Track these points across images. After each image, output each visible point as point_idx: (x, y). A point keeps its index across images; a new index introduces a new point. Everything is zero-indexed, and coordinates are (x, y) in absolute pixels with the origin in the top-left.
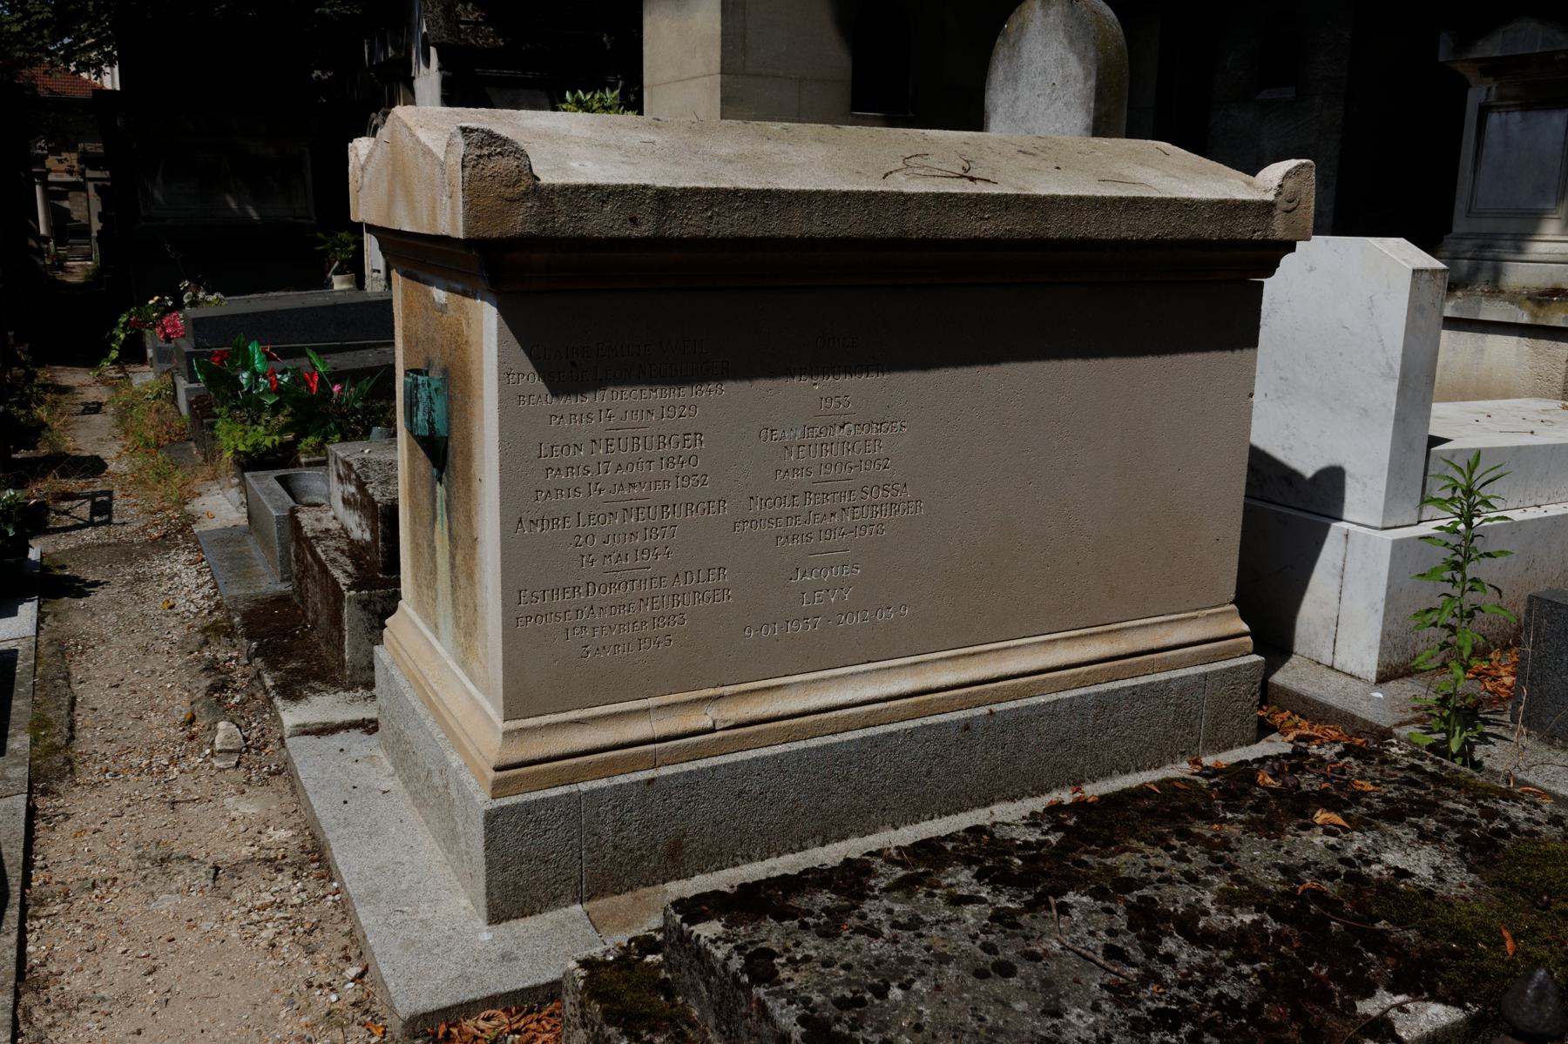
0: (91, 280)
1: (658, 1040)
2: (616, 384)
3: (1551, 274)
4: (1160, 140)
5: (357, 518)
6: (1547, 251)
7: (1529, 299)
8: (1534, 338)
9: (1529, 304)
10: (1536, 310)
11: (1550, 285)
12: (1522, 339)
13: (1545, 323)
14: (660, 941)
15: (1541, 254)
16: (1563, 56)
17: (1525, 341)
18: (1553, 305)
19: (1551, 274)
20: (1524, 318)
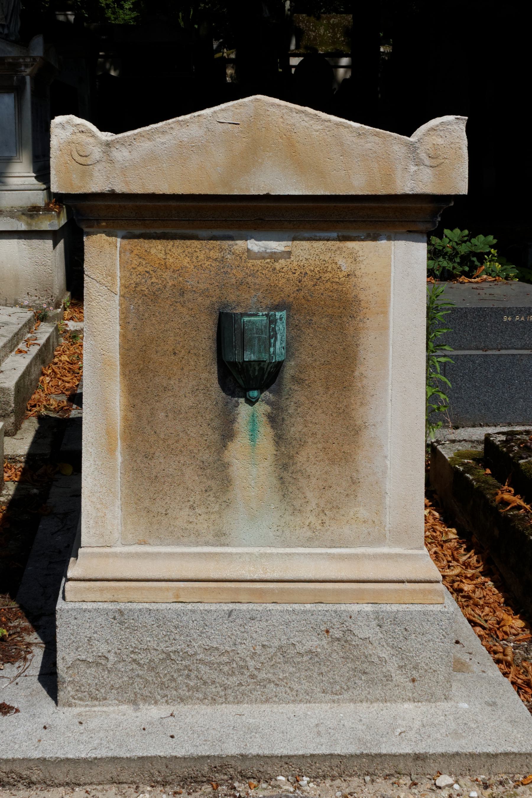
0: (524, 497)
1: (402, 795)
2: (83, 256)
3: (29, 198)
4: (264, 95)
5: (169, 787)
6: (20, 183)
7: (23, 214)
8: (28, 239)
9: (24, 217)
10: (29, 221)
11: (29, 204)
12: (20, 240)
13: (37, 229)
14: (466, 545)
15: (18, 185)
16: (11, 60)
17: (22, 241)
18: (40, 217)
19: (29, 198)
20: (23, 227)
